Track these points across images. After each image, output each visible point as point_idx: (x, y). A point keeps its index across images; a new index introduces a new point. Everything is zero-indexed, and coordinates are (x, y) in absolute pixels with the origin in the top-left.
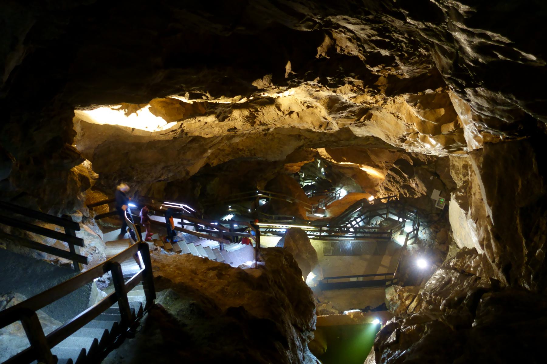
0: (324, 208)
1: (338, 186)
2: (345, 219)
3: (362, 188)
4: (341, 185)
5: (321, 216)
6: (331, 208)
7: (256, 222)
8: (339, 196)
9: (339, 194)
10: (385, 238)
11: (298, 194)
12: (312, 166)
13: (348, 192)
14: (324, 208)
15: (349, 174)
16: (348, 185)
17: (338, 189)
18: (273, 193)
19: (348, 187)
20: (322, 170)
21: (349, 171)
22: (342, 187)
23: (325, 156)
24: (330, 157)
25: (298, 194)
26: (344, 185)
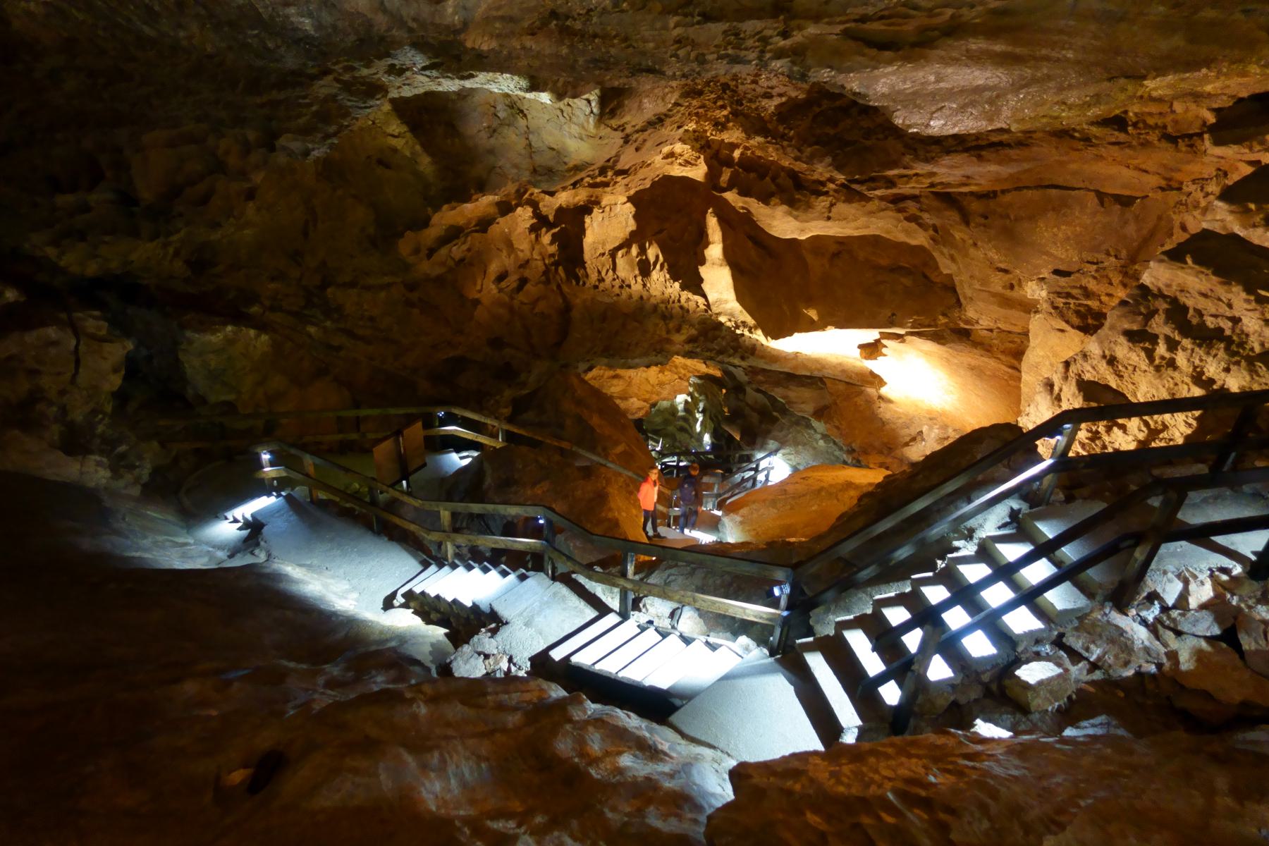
0: (719, 513)
1: (762, 448)
2: (903, 553)
3: (851, 451)
4: (772, 444)
5: (705, 538)
6: (744, 511)
7: (1210, 653)
8: (767, 480)
9: (768, 469)
10: (328, 488)
11: (620, 449)
12: (682, 429)
13: (795, 470)
14: (719, 513)
15: (804, 401)
16: (796, 443)
17: (759, 455)
18: (643, 558)
19: (797, 453)
20: (707, 438)
21: (806, 393)
22: (775, 452)
23: (731, 315)
24: (750, 321)
25: (620, 449)
26: (783, 444)
